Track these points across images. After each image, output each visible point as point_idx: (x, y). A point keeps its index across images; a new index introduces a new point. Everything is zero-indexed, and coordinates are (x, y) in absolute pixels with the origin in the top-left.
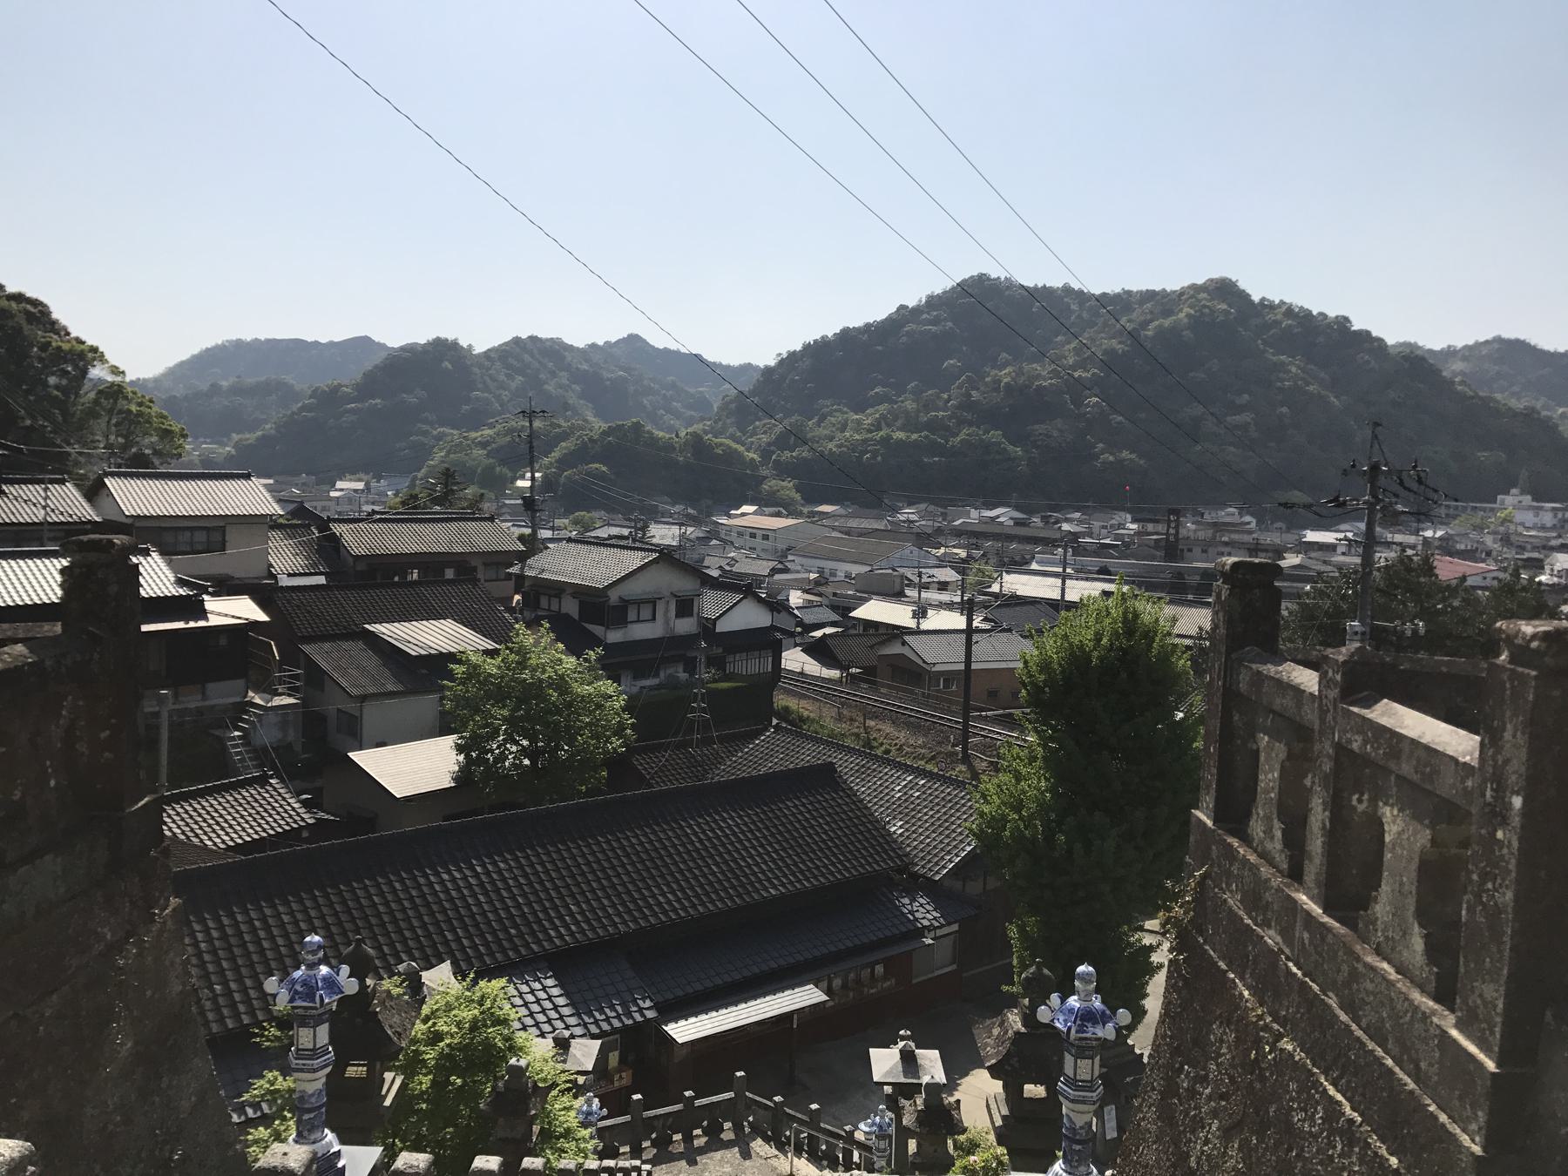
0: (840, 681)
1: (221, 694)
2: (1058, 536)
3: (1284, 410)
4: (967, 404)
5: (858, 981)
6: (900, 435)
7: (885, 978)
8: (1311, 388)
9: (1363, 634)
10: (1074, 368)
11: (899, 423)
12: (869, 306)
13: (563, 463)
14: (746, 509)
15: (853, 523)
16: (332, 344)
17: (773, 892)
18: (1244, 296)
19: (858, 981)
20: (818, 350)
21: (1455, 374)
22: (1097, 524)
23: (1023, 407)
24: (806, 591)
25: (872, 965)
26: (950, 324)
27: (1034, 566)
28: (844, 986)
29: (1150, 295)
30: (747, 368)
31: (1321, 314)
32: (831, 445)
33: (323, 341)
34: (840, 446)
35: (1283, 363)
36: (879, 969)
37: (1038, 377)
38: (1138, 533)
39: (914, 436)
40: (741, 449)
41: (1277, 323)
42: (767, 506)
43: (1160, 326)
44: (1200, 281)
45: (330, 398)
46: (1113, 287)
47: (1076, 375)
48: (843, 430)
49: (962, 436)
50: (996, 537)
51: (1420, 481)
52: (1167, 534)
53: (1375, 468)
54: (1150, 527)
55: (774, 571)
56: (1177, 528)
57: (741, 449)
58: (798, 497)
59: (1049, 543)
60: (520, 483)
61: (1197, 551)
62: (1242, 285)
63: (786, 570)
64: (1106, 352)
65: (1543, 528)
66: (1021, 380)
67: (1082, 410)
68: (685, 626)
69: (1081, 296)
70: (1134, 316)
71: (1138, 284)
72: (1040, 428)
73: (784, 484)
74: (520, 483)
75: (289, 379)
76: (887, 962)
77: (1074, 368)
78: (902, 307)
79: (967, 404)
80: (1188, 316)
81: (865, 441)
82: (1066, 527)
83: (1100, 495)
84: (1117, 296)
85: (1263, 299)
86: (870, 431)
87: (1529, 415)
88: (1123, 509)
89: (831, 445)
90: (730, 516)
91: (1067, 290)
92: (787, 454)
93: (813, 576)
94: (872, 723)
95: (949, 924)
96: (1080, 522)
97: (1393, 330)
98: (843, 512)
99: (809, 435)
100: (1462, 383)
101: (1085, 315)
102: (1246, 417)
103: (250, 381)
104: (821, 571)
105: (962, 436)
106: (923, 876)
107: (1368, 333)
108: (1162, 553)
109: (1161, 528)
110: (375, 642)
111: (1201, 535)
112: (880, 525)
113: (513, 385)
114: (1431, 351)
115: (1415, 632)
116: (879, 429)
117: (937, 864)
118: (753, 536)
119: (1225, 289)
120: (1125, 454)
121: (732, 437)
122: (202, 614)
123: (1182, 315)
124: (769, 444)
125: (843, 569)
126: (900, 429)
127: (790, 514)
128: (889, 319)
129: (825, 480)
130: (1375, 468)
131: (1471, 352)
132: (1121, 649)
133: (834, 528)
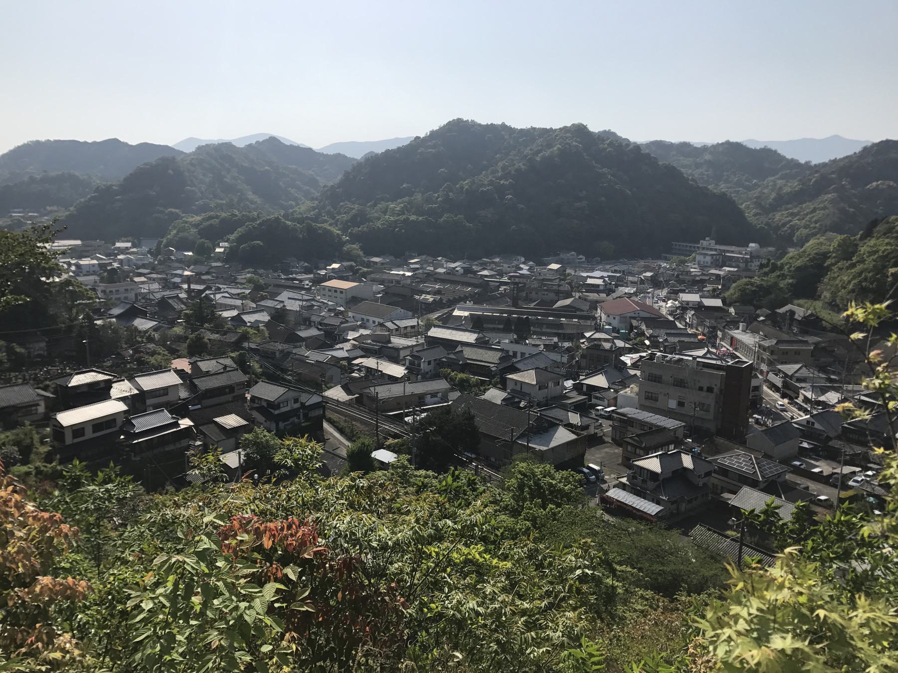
1: (184, 443)
3: (603, 199)
6: (413, 218)
10: (500, 178)
13: (240, 240)
16: (95, 143)
33: (90, 141)
37: (483, 185)
39: (420, 218)
45: (105, 193)
47: (502, 182)
48: (388, 213)
58: (361, 253)
60: (218, 250)
63: (347, 322)
68: (297, 405)
73: (354, 246)
74: (218, 250)
75: (77, 173)
77: (500, 178)
81: (396, 221)
91: (504, 127)
92: (356, 229)
103: (53, 174)
104: (363, 320)
110: (216, 423)
113: (207, 180)
116: (403, 214)
118: (336, 291)
122: (178, 425)
124: (347, 221)
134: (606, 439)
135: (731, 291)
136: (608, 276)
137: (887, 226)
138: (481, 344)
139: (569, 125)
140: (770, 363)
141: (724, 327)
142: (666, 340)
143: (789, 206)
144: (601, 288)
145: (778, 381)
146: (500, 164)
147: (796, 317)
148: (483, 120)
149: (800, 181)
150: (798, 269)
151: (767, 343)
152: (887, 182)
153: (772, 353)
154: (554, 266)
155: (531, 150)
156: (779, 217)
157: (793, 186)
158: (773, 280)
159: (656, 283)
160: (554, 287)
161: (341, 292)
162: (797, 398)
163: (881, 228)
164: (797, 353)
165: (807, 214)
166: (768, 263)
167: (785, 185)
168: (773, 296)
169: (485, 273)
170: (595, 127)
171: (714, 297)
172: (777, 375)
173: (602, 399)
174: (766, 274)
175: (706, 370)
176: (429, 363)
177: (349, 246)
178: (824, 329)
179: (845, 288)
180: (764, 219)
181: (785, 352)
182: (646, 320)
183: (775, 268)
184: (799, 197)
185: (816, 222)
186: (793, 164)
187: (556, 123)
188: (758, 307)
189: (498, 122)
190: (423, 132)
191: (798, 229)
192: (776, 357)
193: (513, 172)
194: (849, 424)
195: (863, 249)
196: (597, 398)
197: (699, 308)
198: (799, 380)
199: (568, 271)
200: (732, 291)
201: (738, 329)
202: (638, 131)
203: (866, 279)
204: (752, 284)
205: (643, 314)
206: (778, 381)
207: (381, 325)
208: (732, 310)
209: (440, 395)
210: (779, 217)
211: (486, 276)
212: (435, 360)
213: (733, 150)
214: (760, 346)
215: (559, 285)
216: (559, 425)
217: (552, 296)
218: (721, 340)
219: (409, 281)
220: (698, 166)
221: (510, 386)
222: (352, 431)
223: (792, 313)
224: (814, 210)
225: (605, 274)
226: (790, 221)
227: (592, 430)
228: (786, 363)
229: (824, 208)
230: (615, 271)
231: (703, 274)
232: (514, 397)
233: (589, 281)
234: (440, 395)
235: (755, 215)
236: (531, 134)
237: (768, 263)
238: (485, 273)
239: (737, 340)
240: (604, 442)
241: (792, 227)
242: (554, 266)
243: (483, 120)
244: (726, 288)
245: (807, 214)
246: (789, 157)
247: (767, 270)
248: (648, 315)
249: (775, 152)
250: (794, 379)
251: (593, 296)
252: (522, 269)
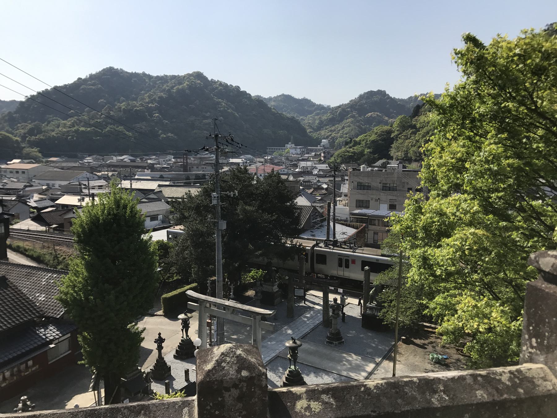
0: (46, 232)
2: (146, 165)
4: (109, 117)
5: (19, 371)
7: (34, 365)
8: (229, 111)
9: (218, 197)
11: (82, 124)
12: (65, 76)
14: (15, 161)
15: (64, 164)
17: (25, 319)
18: (205, 78)
19: (19, 371)
20: (44, 96)
21: (272, 106)
22: (161, 160)
23: (132, 117)
24: (40, 194)
25: (26, 362)
26: (100, 86)
27: (136, 177)
28: (12, 375)
29: (174, 77)
30: (13, 102)
31: (231, 85)
32: (53, 133)
34: (57, 134)
35: (220, 102)
36: (30, 363)
37: (135, 106)
38: (175, 163)
39: (89, 129)
40: (10, 135)
41: (217, 88)
42: (25, 159)
43: (178, 88)
44: (191, 73)
46: (161, 74)
47: (149, 105)
48: (58, 127)
49: (108, 129)
50: (123, 167)
51: (232, 140)
52: (184, 162)
53: (217, 136)
54: (179, 160)
55: (26, 186)
56: (187, 160)
57: (10, 135)
58: (40, 155)
59: (144, 168)
61: (195, 167)
62: (205, 74)
63: (31, 186)
64: (159, 97)
65: (297, 154)
66: (129, 107)
67: (153, 118)
69: (149, 77)
70: (169, 84)
71: (169, 73)
72: (138, 125)
73: (33, 150)
76: (33, 359)
77: (148, 103)
78: (79, 79)
79: (109, 117)
80: (187, 85)
81: (68, 131)
82: (149, 161)
83: (161, 149)
84: (162, 77)
85: (212, 79)
86: (70, 127)
87: (292, 119)
88: (170, 154)
89: (53, 133)
90: (7, 164)
91: (144, 74)
92: (33, 137)
93: (44, 187)
94: (58, 248)
95: (64, 335)
96: (155, 159)
97: (253, 92)
98: (61, 160)
99: (43, 130)
100: (274, 109)
101: (151, 84)
104: (48, 185)
105: (108, 129)
106: (52, 317)
107: (245, 92)
108: (182, 169)
109: (182, 160)
111: (196, 162)
112: (77, 164)
114: (265, 98)
115: (234, 195)
116: (74, 126)
117: (58, 311)
118: (17, 172)
119: (199, 76)
120: (169, 134)
121: (7, 131)
123: (185, 84)
124: (25, 134)
125: (57, 183)
126: (83, 126)
127: (37, 162)
128: (75, 83)
129: (48, 148)
130: (217, 136)
131: (276, 99)
132: (114, 214)
133: (57, 167)
143: (327, 127)
149: (331, 113)
150: (373, 142)
152: (376, 113)
158: (360, 149)
161: (23, 172)
166: (351, 141)
177: (28, 149)
185: (346, 134)
187: (181, 72)
189: (140, 71)
191: (337, 139)
193: (157, 99)
209: (160, 217)
222: (56, 257)
224: (343, 128)
234: (160, 217)
236: (164, 79)
237: (351, 141)
241: (333, 137)
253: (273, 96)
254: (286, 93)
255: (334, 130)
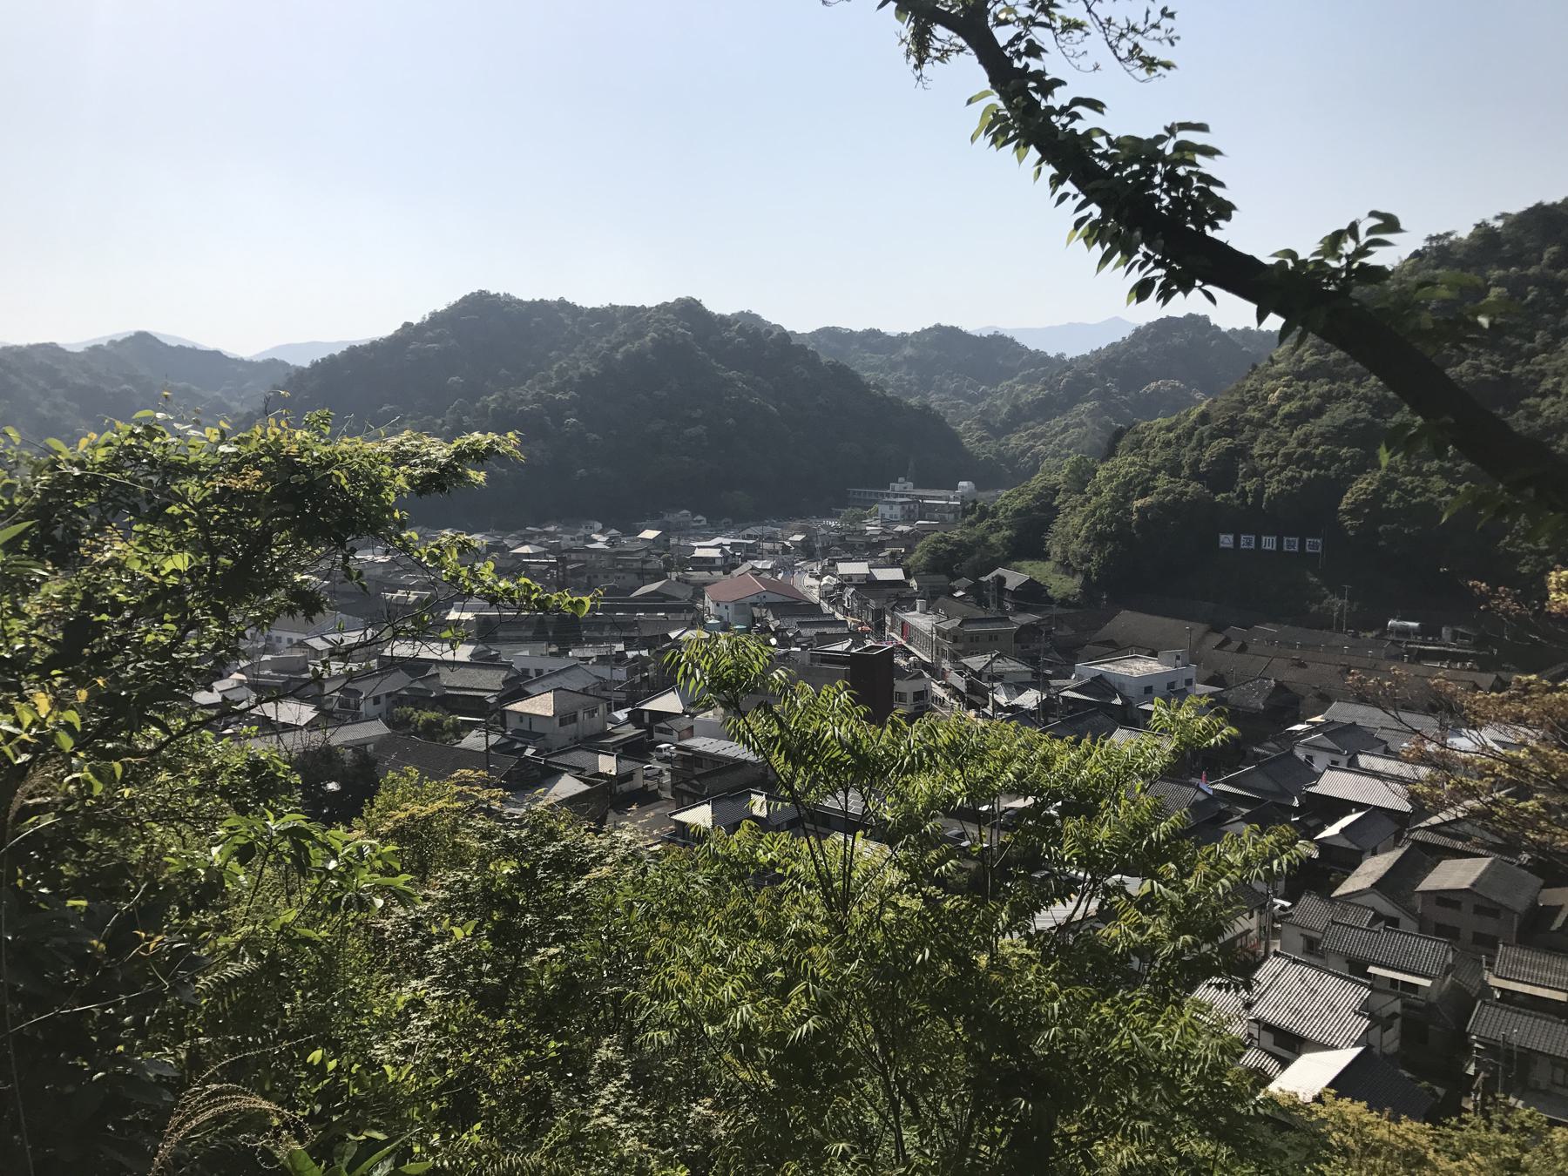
3: (731, 421)
10: (555, 390)
47: (558, 396)
64: (581, 376)
77: (555, 390)
80: (653, 339)
91: (563, 304)
102: (700, 429)
134: (664, 794)
135: (917, 554)
136: (732, 545)
137: (1135, 437)
138: (481, 661)
139: (671, 300)
140: (954, 658)
141: (893, 609)
142: (798, 634)
143: (1031, 423)
144: (718, 563)
145: (960, 683)
146: (556, 367)
147: (1008, 586)
148: (527, 292)
149: (1046, 383)
150: (1018, 512)
151: (947, 626)
153: (955, 640)
154: (650, 534)
155: (608, 342)
156: (1015, 441)
157: (1038, 391)
159: (808, 551)
160: (635, 565)
162: (986, 706)
163: (1125, 442)
164: (993, 637)
165: (1055, 435)
166: (974, 508)
167: (1025, 391)
168: (977, 557)
169: (525, 549)
170: (720, 303)
171: (893, 566)
172: (961, 674)
173: (669, 731)
174: (971, 524)
175: (826, 666)
176: (377, 700)
178: (1051, 600)
179: (1077, 537)
180: (992, 445)
181: (974, 638)
182: (774, 607)
183: (984, 514)
184: (1045, 408)
186: (1039, 358)
188: (954, 577)
189: (551, 296)
190: (417, 315)
191: (1044, 458)
192: (960, 646)
194: (1432, 828)
195: (1101, 474)
196: (661, 730)
197: (868, 585)
198: (994, 678)
199: (673, 541)
200: (919, 556)
201: (914, 609)
202: (797, 312)
203: (1101, 520)
204: (946, 541)
205: (771, 598)
206: (960, 683)
207: (301, 644)
208: (913, 583)
210: (1015, 441)
211: (528, 555)
212: (389, 695)
213: (945, 339)
214: (939, 631)
215: (644, 562)
216: (562, 772)
217: (631, 579)
218: (892, 630)
219: (380, 571)
220: (894, 367)
221: (513, 723)
223: (1001, 580)
224: (1065, 429)
225: (728, 541)
226: (1032, 447)
227: (639, 782)
228: (972, 654)
229: (1080, 425)
230: (749, 537)
231: (883, 533)
232: (514, 741)
233: (699, 553)
235: (980, 440)
236: (608, 317)
237: (974, 508)
238: (525, 549)
239: (910, 626)
240: (659, 799)
241: (1035, 455)
242: (650, 534)
243: (526, 294)
244: (910, 550)
245: (1055, 435)
246: (1032, 348)
247: (972, 518)
248: (779, 599)
249: (1012, 340)
250: (985, 677)
251: (702, 576)
252: (595, 541)
253: (911, 331)
254: (946, 323)
255: (1043, 435)
